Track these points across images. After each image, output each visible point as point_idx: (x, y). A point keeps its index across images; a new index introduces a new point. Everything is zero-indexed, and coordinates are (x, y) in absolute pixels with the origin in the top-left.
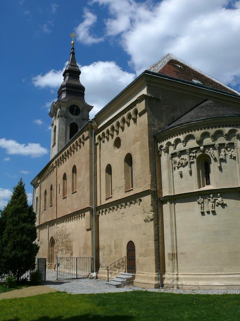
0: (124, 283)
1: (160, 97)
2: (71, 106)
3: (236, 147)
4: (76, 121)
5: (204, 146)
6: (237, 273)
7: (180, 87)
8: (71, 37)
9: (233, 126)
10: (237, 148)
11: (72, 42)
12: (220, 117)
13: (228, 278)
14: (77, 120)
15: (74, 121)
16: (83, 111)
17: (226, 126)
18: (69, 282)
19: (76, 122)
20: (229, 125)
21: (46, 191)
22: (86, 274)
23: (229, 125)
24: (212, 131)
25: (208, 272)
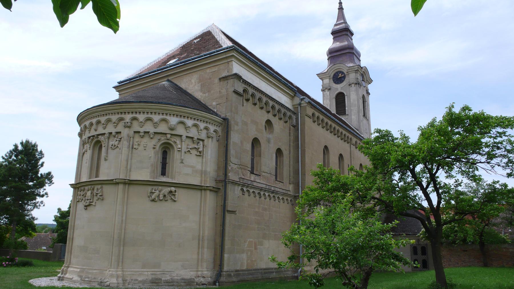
15: (339, 90)
21: (341, 156)
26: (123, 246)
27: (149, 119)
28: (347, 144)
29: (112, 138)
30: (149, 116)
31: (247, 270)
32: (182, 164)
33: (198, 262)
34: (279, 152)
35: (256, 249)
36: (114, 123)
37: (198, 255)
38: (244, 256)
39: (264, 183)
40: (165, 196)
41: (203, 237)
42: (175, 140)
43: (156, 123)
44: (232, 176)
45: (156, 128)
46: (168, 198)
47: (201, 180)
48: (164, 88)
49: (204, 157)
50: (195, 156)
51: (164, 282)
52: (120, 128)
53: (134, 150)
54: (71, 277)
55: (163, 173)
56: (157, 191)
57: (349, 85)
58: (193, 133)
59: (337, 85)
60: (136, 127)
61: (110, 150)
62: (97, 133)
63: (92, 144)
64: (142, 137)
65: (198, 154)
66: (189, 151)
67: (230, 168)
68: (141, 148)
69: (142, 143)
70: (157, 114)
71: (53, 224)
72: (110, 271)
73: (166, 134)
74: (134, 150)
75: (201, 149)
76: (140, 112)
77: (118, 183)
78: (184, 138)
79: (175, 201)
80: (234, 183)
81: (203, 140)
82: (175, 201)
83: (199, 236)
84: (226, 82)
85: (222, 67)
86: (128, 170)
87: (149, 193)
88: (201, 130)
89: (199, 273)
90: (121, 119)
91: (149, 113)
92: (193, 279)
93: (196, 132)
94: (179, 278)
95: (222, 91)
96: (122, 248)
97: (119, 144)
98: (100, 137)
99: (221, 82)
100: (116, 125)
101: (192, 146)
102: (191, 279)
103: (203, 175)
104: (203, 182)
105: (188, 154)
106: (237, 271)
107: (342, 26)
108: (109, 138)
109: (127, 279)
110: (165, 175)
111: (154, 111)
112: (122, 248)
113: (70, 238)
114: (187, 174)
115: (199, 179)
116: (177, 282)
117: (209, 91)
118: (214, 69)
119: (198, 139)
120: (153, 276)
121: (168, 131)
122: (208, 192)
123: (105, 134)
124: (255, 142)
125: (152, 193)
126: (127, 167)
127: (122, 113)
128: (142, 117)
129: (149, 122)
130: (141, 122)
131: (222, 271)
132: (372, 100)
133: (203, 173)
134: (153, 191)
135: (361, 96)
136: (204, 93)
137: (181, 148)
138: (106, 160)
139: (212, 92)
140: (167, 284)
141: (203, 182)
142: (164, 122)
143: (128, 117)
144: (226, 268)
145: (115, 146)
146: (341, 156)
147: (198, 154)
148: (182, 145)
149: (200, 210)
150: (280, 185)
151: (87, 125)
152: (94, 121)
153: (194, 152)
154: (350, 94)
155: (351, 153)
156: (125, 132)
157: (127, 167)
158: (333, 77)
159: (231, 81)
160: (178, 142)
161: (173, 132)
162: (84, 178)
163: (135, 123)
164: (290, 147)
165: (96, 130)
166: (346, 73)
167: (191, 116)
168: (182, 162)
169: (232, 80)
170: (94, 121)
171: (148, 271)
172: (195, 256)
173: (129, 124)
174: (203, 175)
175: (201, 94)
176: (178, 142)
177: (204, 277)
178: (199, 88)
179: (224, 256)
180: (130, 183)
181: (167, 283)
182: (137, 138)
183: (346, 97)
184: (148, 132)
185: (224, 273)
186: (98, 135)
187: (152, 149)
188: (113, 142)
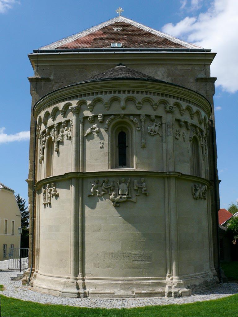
0: (21, 276)
1: (52, 77)
3: (71, 124)
5: (48, 128)
6: (113, 278)
8: (118, 13)
9: (66, 99)
10: (72, 126)
12: (54, 92)
13: (104, 284)
17: (60, 101)
18: (11, 272)
22: (16, 266)
23: (146, 92)
25: (123, 277)
27: (147, 100)
52: (160, 112)
54: (112, 292)
63: (113, 123)
70: (140, 93)
71: (226, 211)
72: (172, 279)
77: (169, 177)
85: (197, 68)
88: (183, 110)
98: (131, 117)
111: (105, 90)
118: (186, 68)
122: (173, 182)
127: (166, 95)
129: (163, 105)
145: (155, 132)
151: (50, 112)
152: (61, 105)
186: (125, 115)
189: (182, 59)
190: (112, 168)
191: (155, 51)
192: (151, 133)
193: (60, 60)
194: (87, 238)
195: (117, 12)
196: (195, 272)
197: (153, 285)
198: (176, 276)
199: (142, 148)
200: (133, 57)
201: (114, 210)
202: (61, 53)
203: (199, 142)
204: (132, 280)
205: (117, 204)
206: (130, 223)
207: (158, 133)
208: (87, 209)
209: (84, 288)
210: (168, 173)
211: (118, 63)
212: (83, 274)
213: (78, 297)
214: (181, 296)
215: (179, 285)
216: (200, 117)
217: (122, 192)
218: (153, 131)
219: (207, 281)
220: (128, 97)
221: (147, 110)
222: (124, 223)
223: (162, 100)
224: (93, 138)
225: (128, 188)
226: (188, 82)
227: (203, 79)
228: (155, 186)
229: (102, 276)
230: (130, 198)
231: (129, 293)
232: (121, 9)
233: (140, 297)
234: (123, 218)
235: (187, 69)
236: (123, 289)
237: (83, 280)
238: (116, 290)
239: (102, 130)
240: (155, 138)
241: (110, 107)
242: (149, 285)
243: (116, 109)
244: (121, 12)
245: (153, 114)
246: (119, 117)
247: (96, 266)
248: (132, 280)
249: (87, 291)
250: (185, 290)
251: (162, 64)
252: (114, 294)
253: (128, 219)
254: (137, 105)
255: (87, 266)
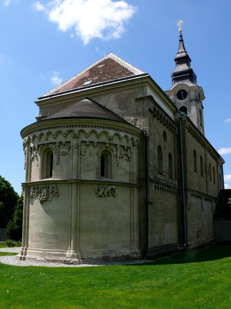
2: (178, 92)
4: (184, 104)
7: (67, 98)
8: (178, 25)
11: (179, 30)
14: (184, 103)
15: (182, 105)
16: (189, 93)
19: (185, 105)
20: (88, 126)
21: (201, 157)
24: (54, 131)
26: (79, 233)
28: (203, 148)
29: (61, 147)
30: (93, 129)
31: (159, 247)
32: (118, 167)
33: (131, 242)
34: (170, 155)
35: (162, 230)
36: (65, 134)
37: (131, 237)
38: (157, 236)
39: (164, 180)
40: (108, 193)
41: (133, 223)
42: (112, 148)
43: (99, 135)
44: (151, 176)
45: (98, 139)
46: (110, 194)
47: (130, 180)
48: (87, 104)
49: (131, 161)
50: (125, 161)
51: (112, 259)
53: (82, 156)
55: (103, 174)
56: (103, 189)
57: (190, 101)
58: (124, 142)
59: (180, 100)
60: (83, 138)
61: (61, 156)
62: (48, 142)
63: (43, 150)
64: (88, 146)
65: (128, 159)
66: (122, 157)
67: (149, 170)
68: (87, 154)
69: (88, 151)
72: (70, 252)
73: (106, 143)
74: (82, 156)
75: (129, 156)
76: (86, 126)
78: (118, 146)
79: (115, 196)
80: (152, 181)
81: (130, 148)
82: (115, 196)
83: (131, 222)
84: (142, 102)
85: (137, 90)
86: (78, 172)
87: (96, 191)
89: (133, 250)
90: (71, 131)
91: (81, 126)
92: (130, 255)
93: (126, 141)
94: (121, 255)
95: (138, 109)
96: (78, 234)
97: (68, 151)
98: (51, 145)
99: (137, 102)
100: (87, 136)
101: (124, 152)
102: (128, 255)
103: (131, 176)
104: (131, 181)
105: (121, 159)
106: (155, 248)
107: (184, 54)
108: (59, 146)
109: (84, 257)
110: (104, 176)
112: (78, 234)
113: (25, 226)
114: (121, 175)
115: (128, 178)
116: (121, 258)
117: (126, 109)
118: (129, 92)
119: (127, 147)
120: (104, 255)
121: (108, 141)
123: (56, 143)
124: (160, 148)
125: (99, 190)
126: (77, 170)
128: (87, 130)
130: (87, 134)
131: (147, 248)
132: (204, 112)
133: (131, 173)
134: (100, 189)
135: (199, 109)
136: (122, 110)
137: (117, 155)
138: (58, 164)
139: (129, 109)
140: (114, 260)
141: (131, 181)
142: (93, 134)
143: (76, 130)
144: (149, 246)
145: (65, 153)
146: (201, 157)
147: (128, 159)
148: (117, 153)
149: (131, 203)
150: (171, 181)
153: (125, 157)
154: (191, 108)
155: (205, 155)
156: (74, 142)
157: (77, 170)
158: (177, 94)
159: (146, 102)
160: (115, 150)
161: (111, 142)
162: (36, 178)
163: (82, 135)
164: (175, 151)
165: (47, 140)
166: (187, 92)
167: (123, 129)
168: (118, 166)
169: (147, 100)
170: (45, 132)
171: (99, 251)
172: (129, 238)
173: (78, 135)
174: (131, 176)
175: (120, 110)
176: (115, 150)
177: (136, 254)
178: (117, 106)
179: (148, 237)
180: (80, 183)
181: (114, 259)
182: (84, 147)
183: (188, 110)
184: (93, 142)
185: (149, 250)
186: (48, 144)
187: (96, 156)
188: (63, 150)
189: (125, 86)
190: (42, 179)
191: (108, 83)
192: (63, 154)
193: (52, 102)
194: (30, 224)
195: (178, 25)
196: (95, 249)
197: (58, 255)
198: (73, 250)
199: (57, 164)
200: (109, 87)
201: (40, 205)
202: (53, 97)
203: (112, 153)
204: (47, 251)
205: (42, 202)
206: (48, 214)
207: (68, 153)
208: (31, 205)
209: (26, 255)
210: (69, 181)
211: (85, 97)
212: (27, 246)
213: (20, 260)
214: (72, 264)
215: (73, 256)
216: (108, 135)
217: (43, 194)
218: (64, 152)
219: (109, 257)
220: (48, 132)
221: (61, 138)
222: (45, 214)
223: (92, 130)
224: (34, 160)
225: (47, 191)
226: (131, 103)
227: (140, 98)
228: (63, 189)
229: (34, 248)
230: (48, 198)
231: (43, 259)
232: (181, 21)
233: (48, 262)
234: (44, 211)
235: (130, 92)
236: (41, 256)
237: (26, 249)
238: (37, 257)
239: (38, 155)
240: (65, 157)
241: (40, 140)
242: (55, 255)
243: (43, 141)
244: (181, 24)
245: (64, 140)
246: (45, 146)
247: (32, 241)
248: (47, 251)
249: (26, 256)
250: (77, 260)
251: (112, 92)
252: (36, 259)
253: (47, 212)
254: (53, 136)
255: (29, 241)
